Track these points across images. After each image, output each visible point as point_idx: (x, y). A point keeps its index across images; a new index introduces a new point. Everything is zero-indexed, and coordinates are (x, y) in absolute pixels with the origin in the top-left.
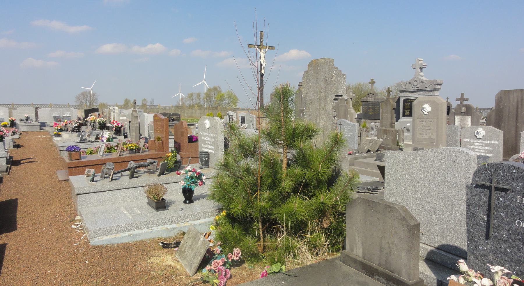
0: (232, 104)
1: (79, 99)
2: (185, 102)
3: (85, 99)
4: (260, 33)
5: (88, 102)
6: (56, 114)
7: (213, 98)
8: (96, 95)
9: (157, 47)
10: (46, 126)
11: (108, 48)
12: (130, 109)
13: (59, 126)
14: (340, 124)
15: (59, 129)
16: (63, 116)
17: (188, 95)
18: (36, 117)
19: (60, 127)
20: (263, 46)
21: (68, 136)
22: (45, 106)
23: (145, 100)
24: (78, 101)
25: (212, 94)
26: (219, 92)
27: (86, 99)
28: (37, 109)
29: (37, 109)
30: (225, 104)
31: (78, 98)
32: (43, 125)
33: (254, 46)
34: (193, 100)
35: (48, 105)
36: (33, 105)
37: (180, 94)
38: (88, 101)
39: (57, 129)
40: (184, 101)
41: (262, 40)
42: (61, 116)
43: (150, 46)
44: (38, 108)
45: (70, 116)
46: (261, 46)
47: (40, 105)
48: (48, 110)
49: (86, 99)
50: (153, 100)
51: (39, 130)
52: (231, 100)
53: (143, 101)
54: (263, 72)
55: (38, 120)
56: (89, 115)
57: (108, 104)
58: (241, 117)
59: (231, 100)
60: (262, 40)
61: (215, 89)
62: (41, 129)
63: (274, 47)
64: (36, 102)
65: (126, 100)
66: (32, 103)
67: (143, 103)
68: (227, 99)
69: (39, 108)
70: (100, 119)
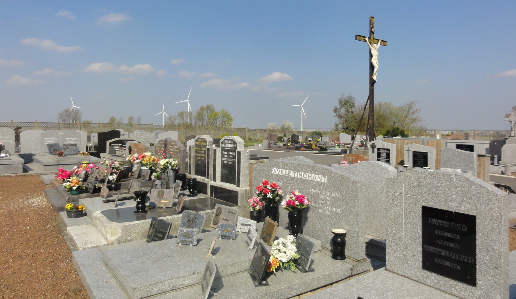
0: (227, 124)
1: (62, 116)
2: (174, 121)
3: (68, 117)
4: (370, 20)
5: (71, 119)
6: (52, 140)
7: (206, 116)
8: (79, 112)
9: (145, 67)
10: (34, 161)
11: (95, 67)
12: (405, 153)
13: (75, 181)
14: (410, 152)
15: (74, 188)
16: (64, 145)
17: (178, 113)
18: (15, 142)
19: (77, 183)
20: (374, 39)
21: (120, 230)
22: (30, 126)
23: (132, 118)
24: (61, 118)
25: (205, 113)
26: (212, 111)
27: (70, 117)
28: (17, 130)
29: (17, 130)
30: (218, 123)
31: (61, 115)
32: (28, 158)
33: (363, 38)
34: (183, 119)
35: (33, 123)
36: (13, 122)
37: (163, 113)
38: (72, 119)
39: (71, 189)
40: (172, 119)
41: (373, 30)
42: (61, 144)
43: (138, 66)
44: (20, 128)
45: (76, 145)
46: (373, 39)
47: (22, 122)
48: (37, 133)
49: (70, 117)
50: (140, 118)
51: (21, 171)
52: (226, 119)
53: (129, 119)
54: (374, 77)
55: (20, 146)
56: (107, 142)
57: (123, 123)
58: (414, 152)
59: (226, 119)
60: (373, 30)
61: (208, 108)
62: (26, 170)
63: (386, 42)
64: (19, 119)
65: (112, 118)
66: (12, 120)
67: (129, 121)
68: (221, 118)
69: (20, 128)
70: (166, 160)
